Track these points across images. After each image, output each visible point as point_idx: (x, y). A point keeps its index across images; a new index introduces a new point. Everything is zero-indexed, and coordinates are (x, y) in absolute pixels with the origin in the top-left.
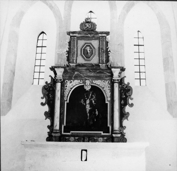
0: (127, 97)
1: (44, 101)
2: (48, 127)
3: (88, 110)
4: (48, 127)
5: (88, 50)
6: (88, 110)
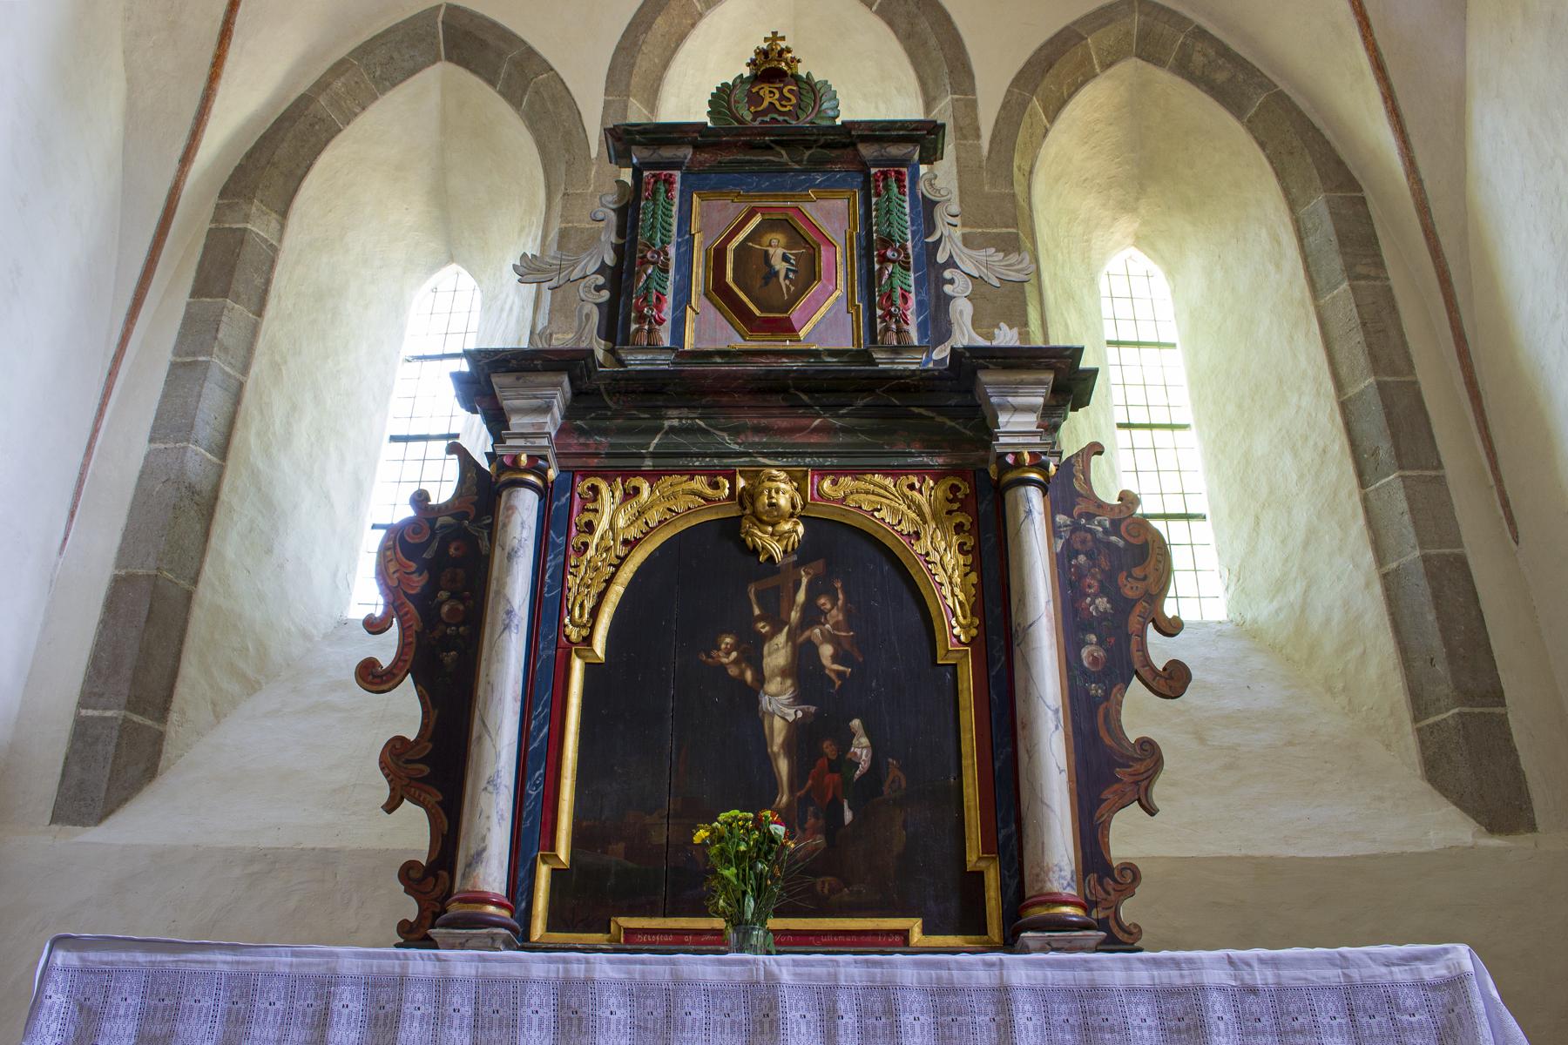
0: (1123, 607)
1: (386, 649)
2: (410, 875)
3: (778, 732)
4: (410, 875)
5: (776, 254)
6: (778, 732)
